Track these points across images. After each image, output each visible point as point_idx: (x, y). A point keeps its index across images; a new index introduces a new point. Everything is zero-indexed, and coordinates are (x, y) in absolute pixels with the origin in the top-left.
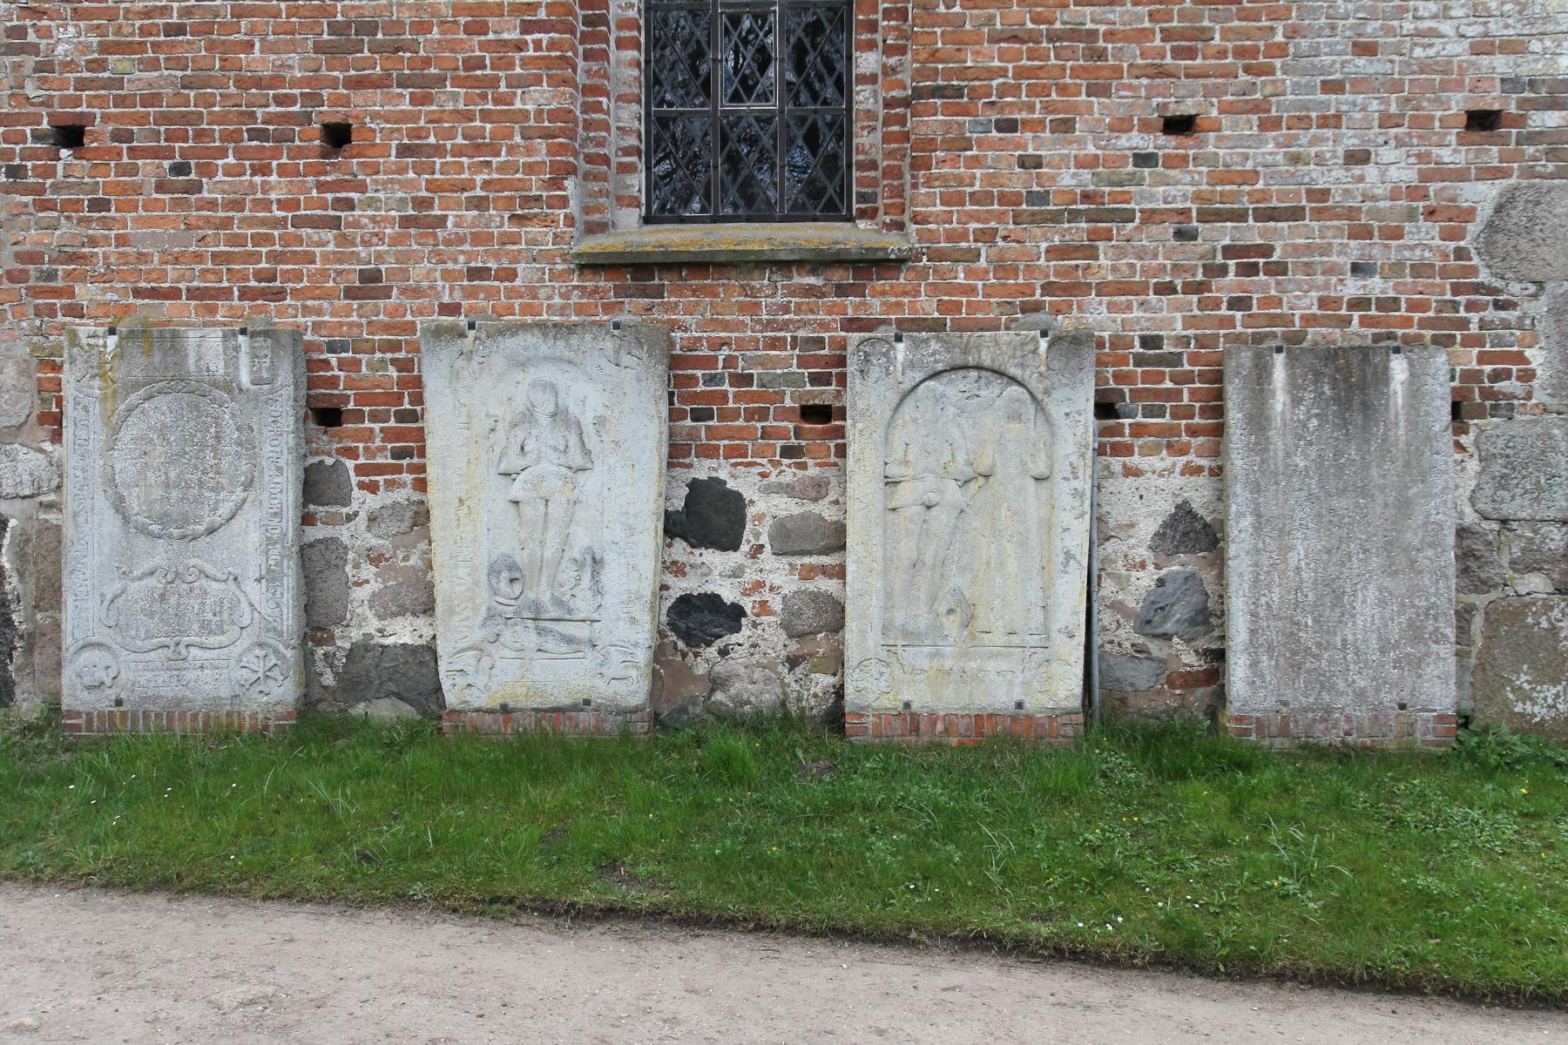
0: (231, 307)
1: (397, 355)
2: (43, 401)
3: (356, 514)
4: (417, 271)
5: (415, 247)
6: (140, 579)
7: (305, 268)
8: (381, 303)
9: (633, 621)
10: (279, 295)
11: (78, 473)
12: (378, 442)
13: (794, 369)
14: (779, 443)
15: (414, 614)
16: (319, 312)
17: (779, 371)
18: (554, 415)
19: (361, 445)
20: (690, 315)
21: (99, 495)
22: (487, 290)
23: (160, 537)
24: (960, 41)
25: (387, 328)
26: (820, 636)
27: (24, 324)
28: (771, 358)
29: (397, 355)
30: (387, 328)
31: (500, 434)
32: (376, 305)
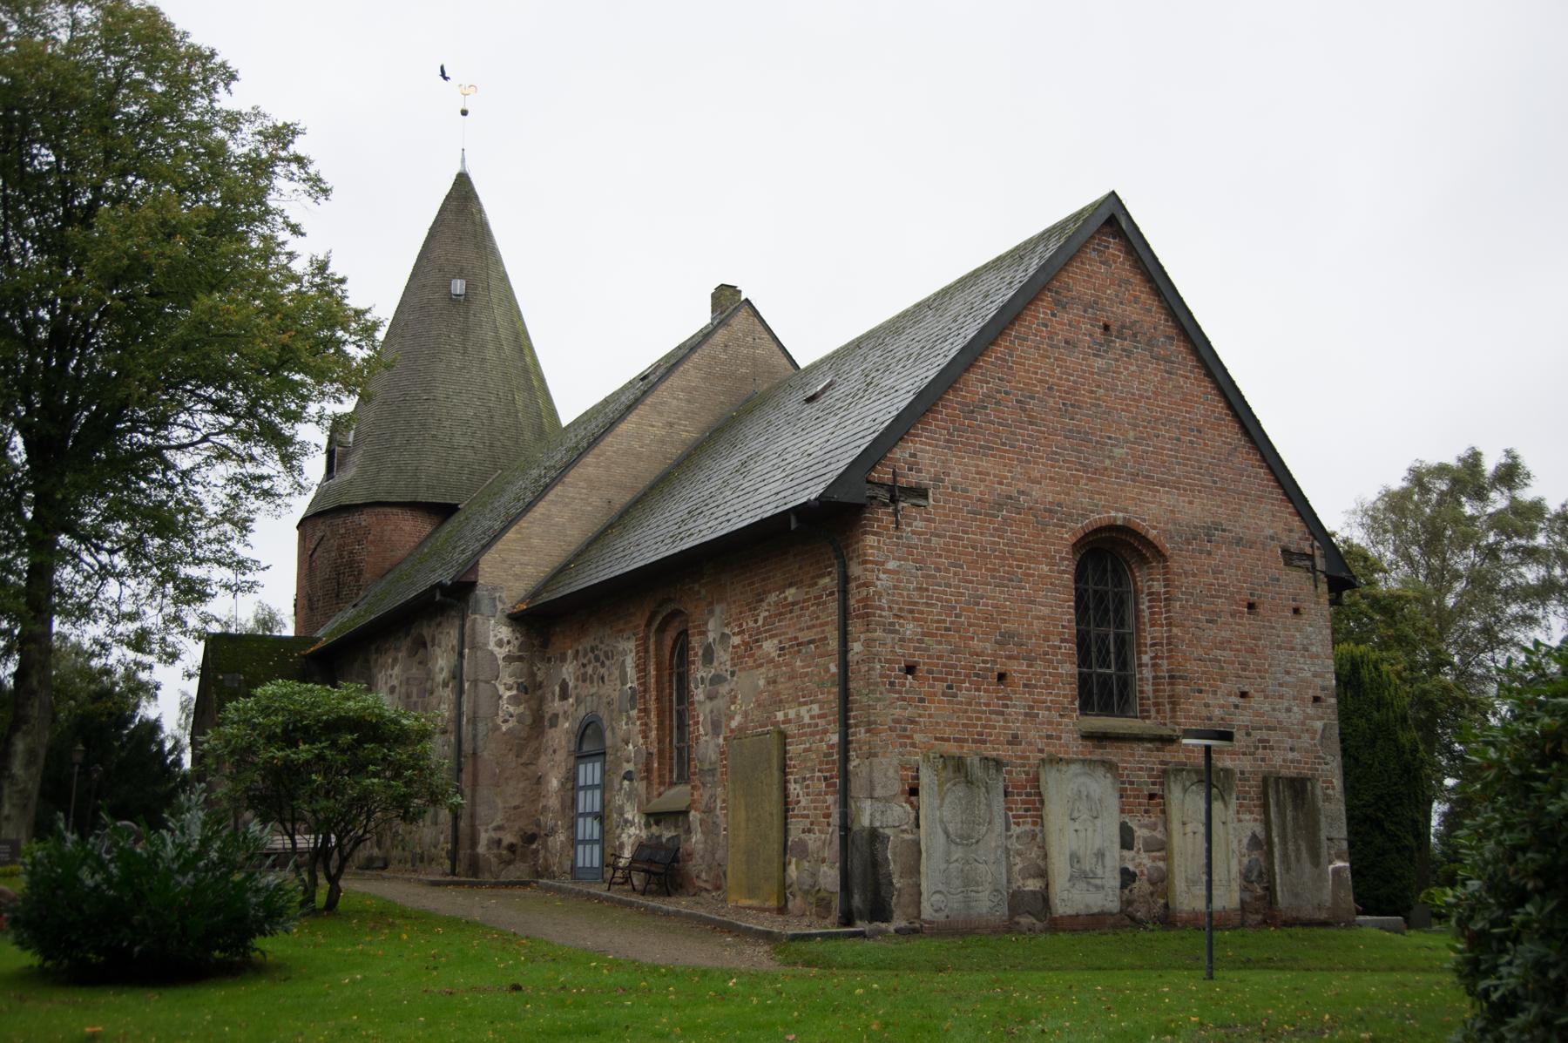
10: (984, 742)
20: (1112, 753)
25: (1021, 758)
30: (1021, 758)
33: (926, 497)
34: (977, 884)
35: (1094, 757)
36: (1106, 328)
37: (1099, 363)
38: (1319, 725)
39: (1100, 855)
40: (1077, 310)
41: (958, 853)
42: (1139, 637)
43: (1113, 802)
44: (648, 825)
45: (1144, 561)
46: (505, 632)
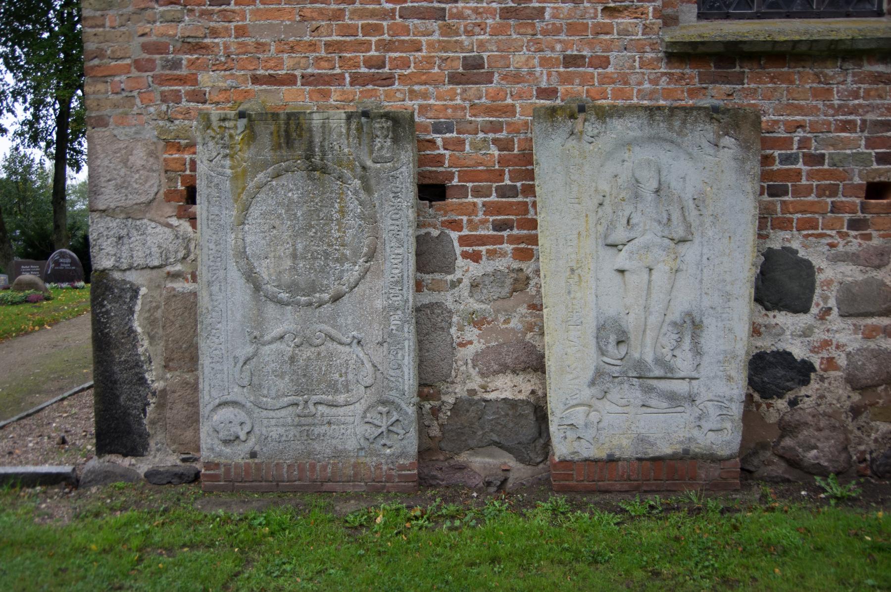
0: (344, 92)
1: (498, 136)
2: (170, 179)
3: (460, 281)
4: (517, 58)
5: (514, 36)
6: (270, 343)
7: (413, 56)
8: (483, 88)
9: (729, 378)
10: (388, 80)
11: (212, 246)
12: (481, 216)
13: (862, 149)
14: (847, 216)
15: (514, 372)
16: (425, 96)
17: (848, 152)
18: (657, 191)
19: (465, 218)
20: (766, 97)
21: (232, 266)
22: (582, 76)
23: (288, 304)
25: (489, 111)
26: (880, 389)
27: (152, 109)
28: (842, 140)
29: (498, 136)
30: (489, 111)
31: (608, 208)
32: (478, 89)
34: (333, 388)
39: (692, 325)
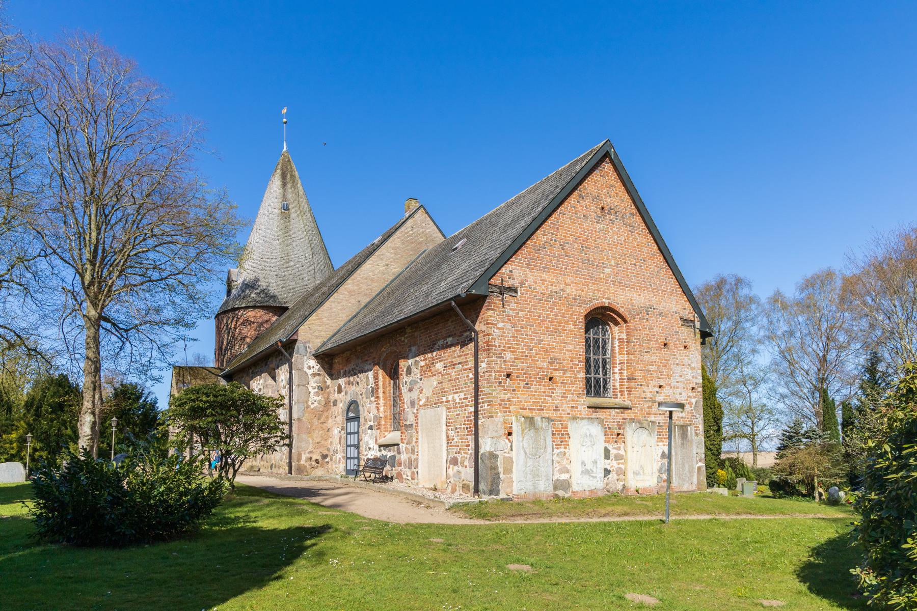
20: (601, 414)
24: (635, 370)
33: (516, 292)
35: (593, 416)
36: (603, 208)
37: (599, 226)
38: (694, 401)
39: (595, 462)
40: (588, 200)
41: (530, 463)
42: (613, 360)
43: (602, 438)
44: (380, 451)
45: (617, 323)
46: (312, 362)
